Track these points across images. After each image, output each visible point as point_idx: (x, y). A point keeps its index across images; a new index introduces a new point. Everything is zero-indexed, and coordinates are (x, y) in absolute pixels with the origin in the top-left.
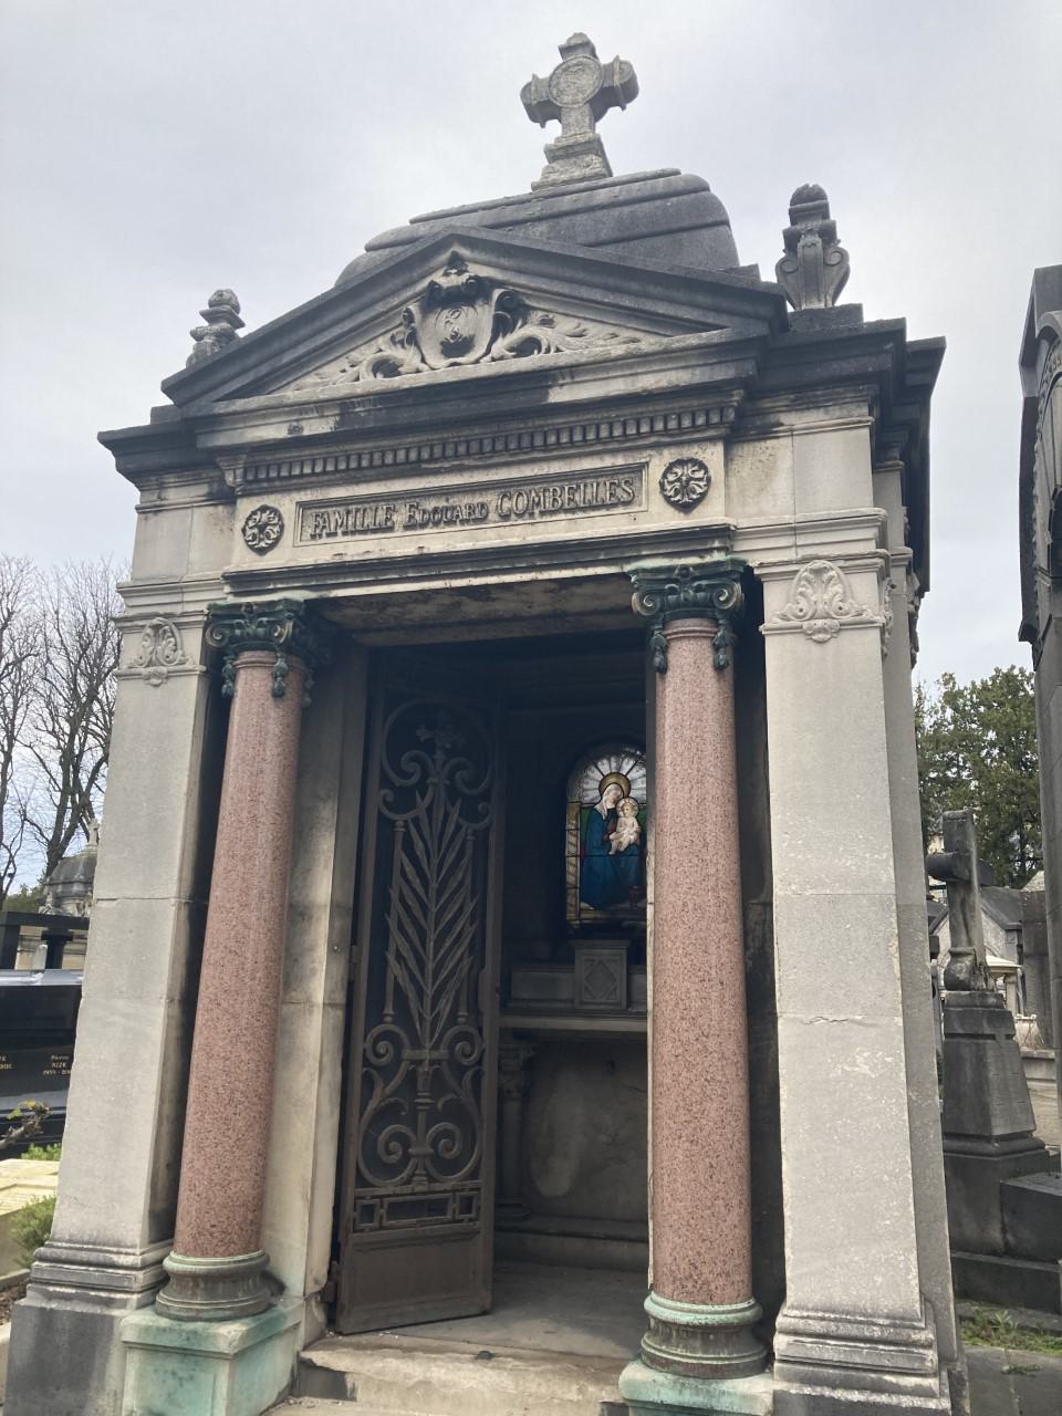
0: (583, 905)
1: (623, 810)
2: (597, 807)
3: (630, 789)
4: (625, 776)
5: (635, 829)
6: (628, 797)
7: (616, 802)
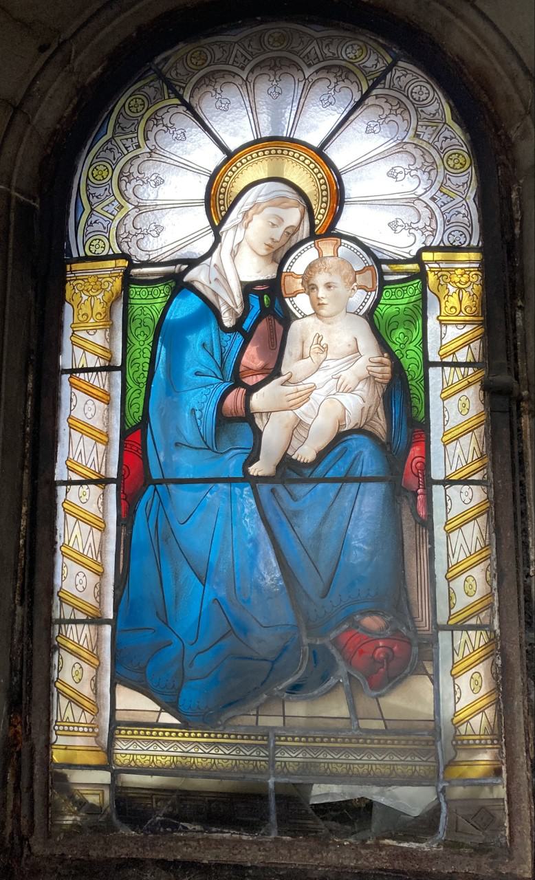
0: (133, 702)
1: (310, 287)
2: (198, 275)
3: (338, 198)
5: (361, 366)
6: (330, 232)
7: (281, 255)
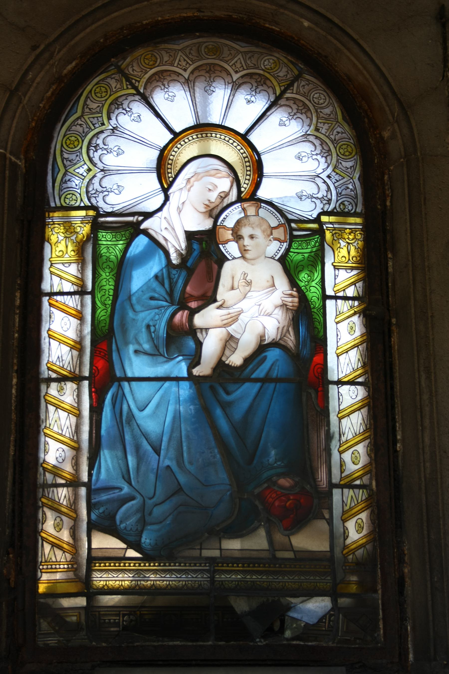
0: (104, 542)
1: (238, 237)
4: (176, 136)
